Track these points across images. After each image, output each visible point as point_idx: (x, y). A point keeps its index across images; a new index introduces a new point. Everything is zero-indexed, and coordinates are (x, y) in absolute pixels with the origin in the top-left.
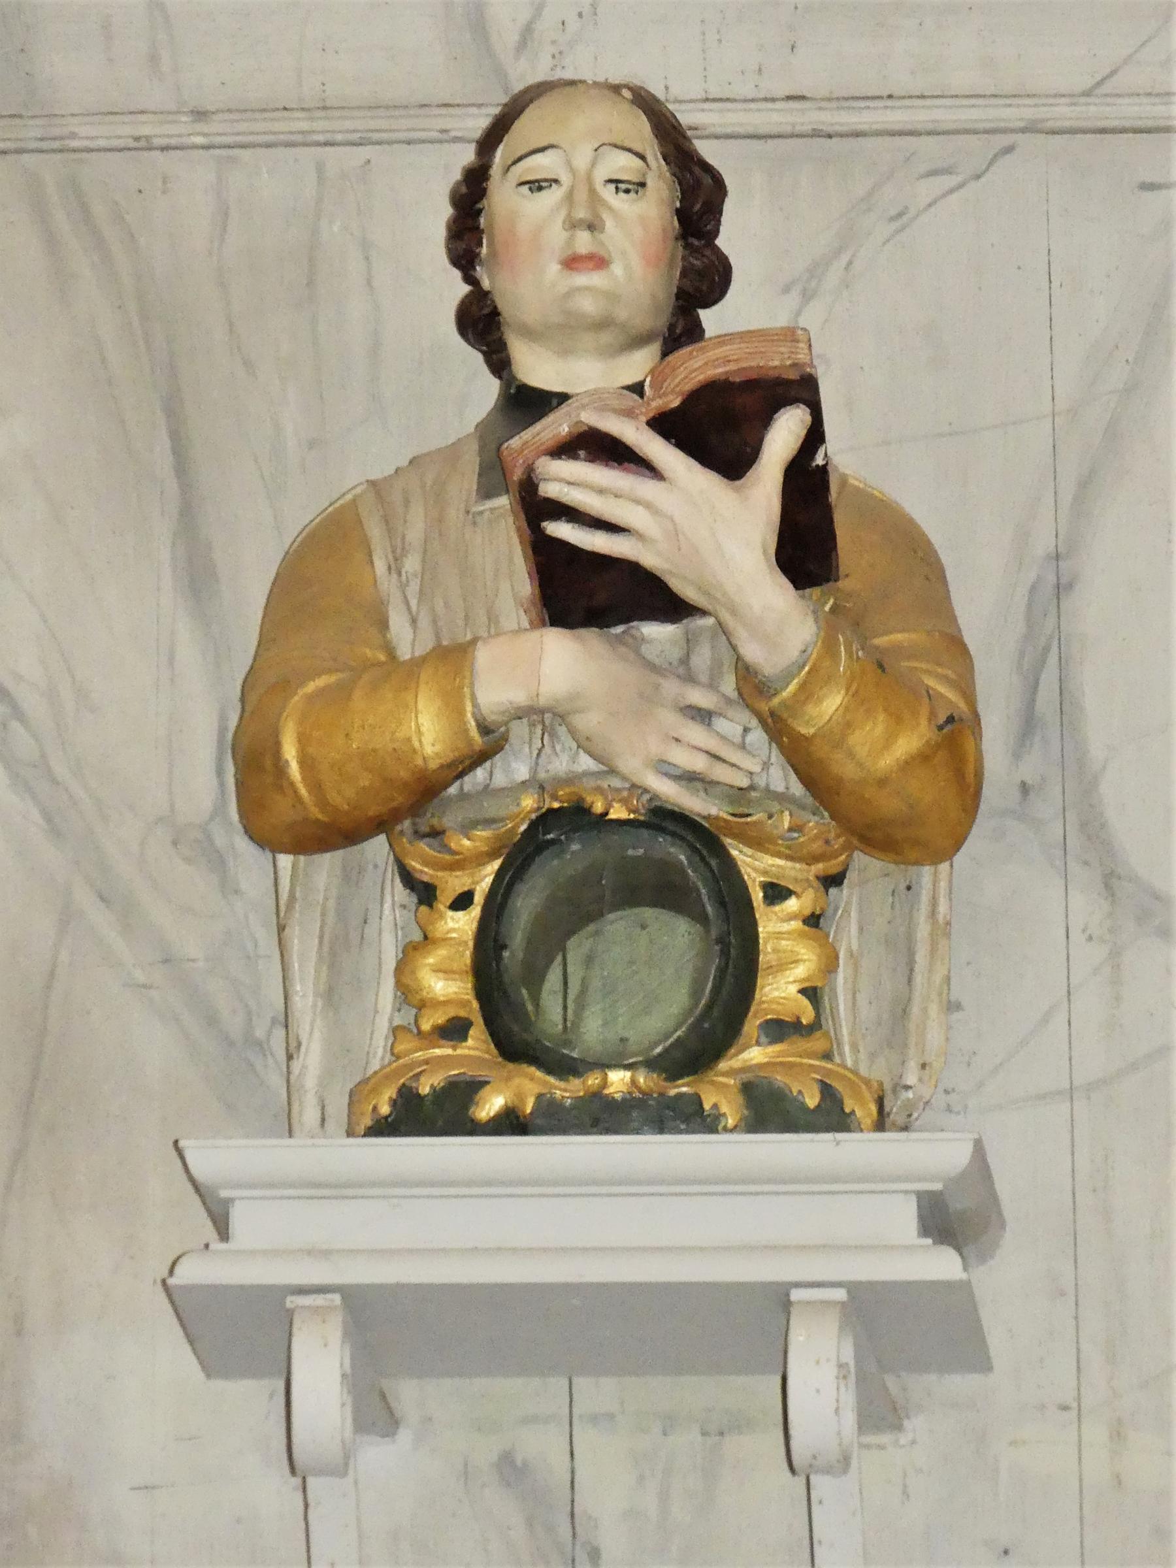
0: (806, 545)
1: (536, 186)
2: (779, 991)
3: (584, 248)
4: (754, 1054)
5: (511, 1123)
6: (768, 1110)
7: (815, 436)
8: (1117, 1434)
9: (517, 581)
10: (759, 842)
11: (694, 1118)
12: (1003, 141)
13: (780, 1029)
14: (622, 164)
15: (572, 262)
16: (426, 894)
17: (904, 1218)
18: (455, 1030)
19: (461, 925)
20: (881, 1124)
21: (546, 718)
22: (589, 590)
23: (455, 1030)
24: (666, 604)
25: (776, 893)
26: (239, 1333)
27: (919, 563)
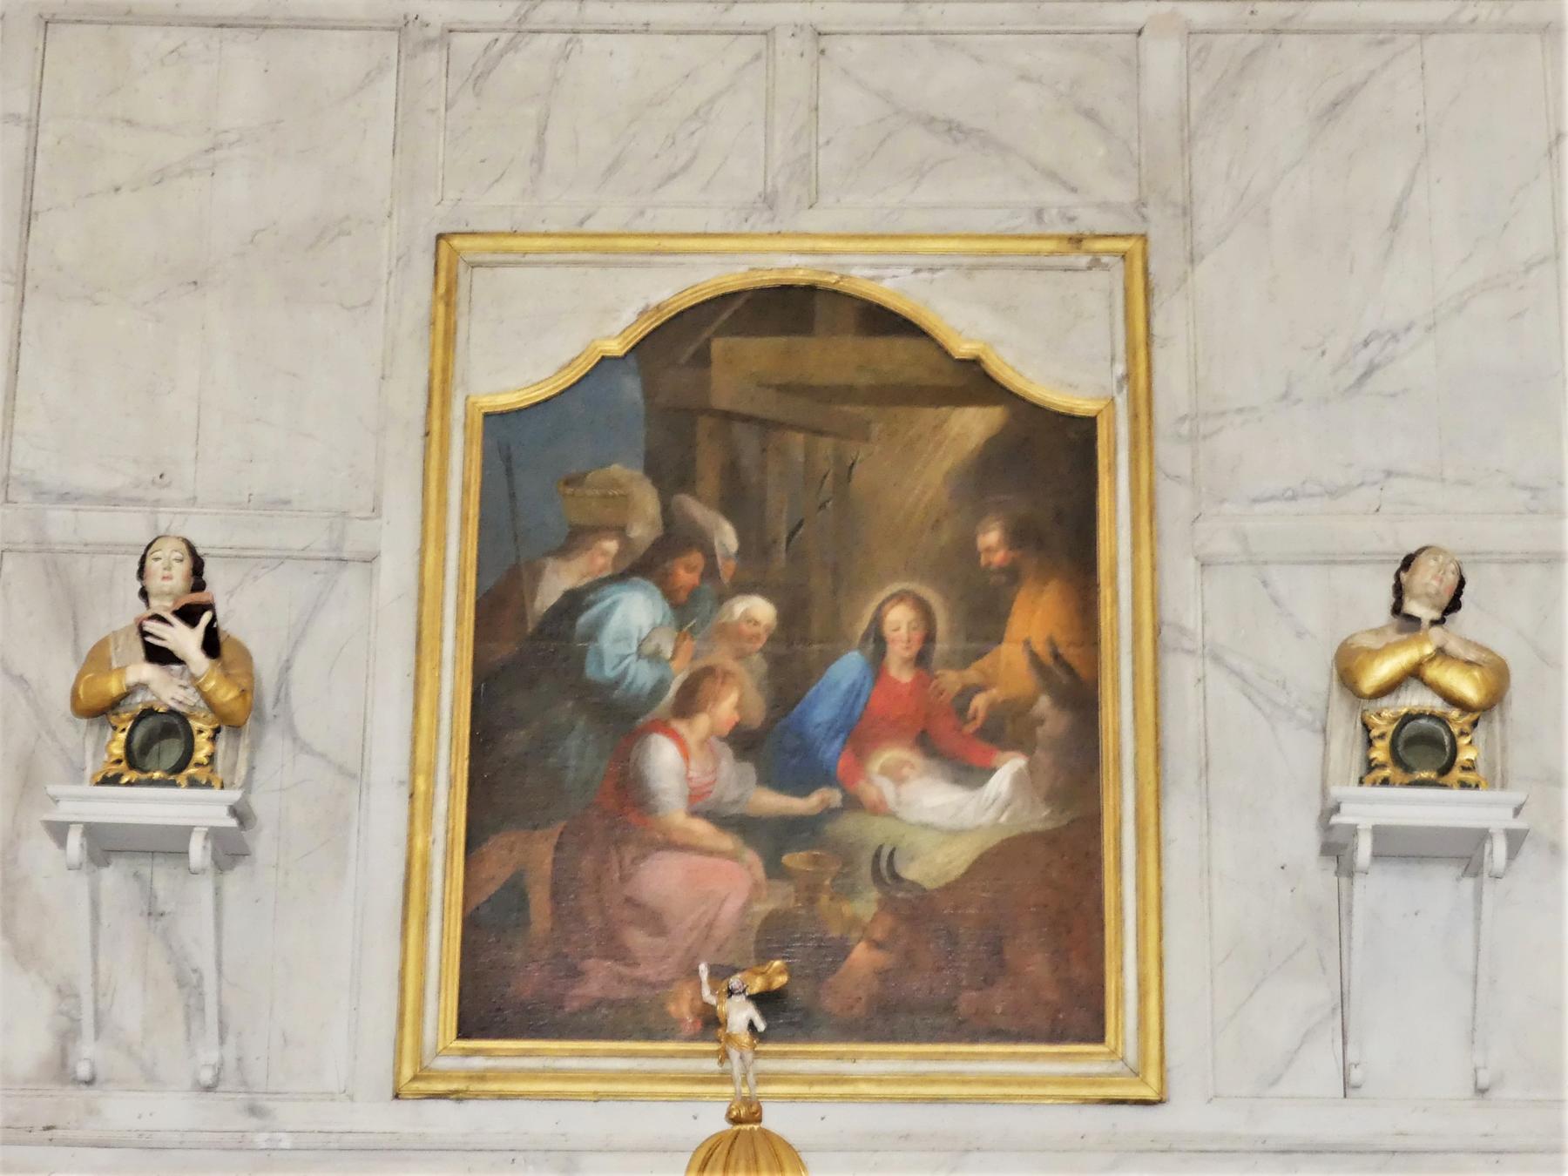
0: (212, 644)
1: (157, 559)
2: (200, 755)
3: (170, 579)
4: (191, 770)
5: (129, 784)
6: (193, 783)
7: (214, 619)
8: (287, 874)
9: (141, 654)
10: (197, 719)
11: (173, 784)
12: (282, 560)
13: (198, 765)
14: (178, 555)
15: (164, 578)
16: (115, 728)
17: (224, 811)
18: (119, 761)
19: (123, 736)
20: (222, 787)
21: (143, 686)
22: (159, 655)
23: (119, 761)
24: (180, 662)
25: (200, 732)
26: (58, 832)
27: (245, 656)
